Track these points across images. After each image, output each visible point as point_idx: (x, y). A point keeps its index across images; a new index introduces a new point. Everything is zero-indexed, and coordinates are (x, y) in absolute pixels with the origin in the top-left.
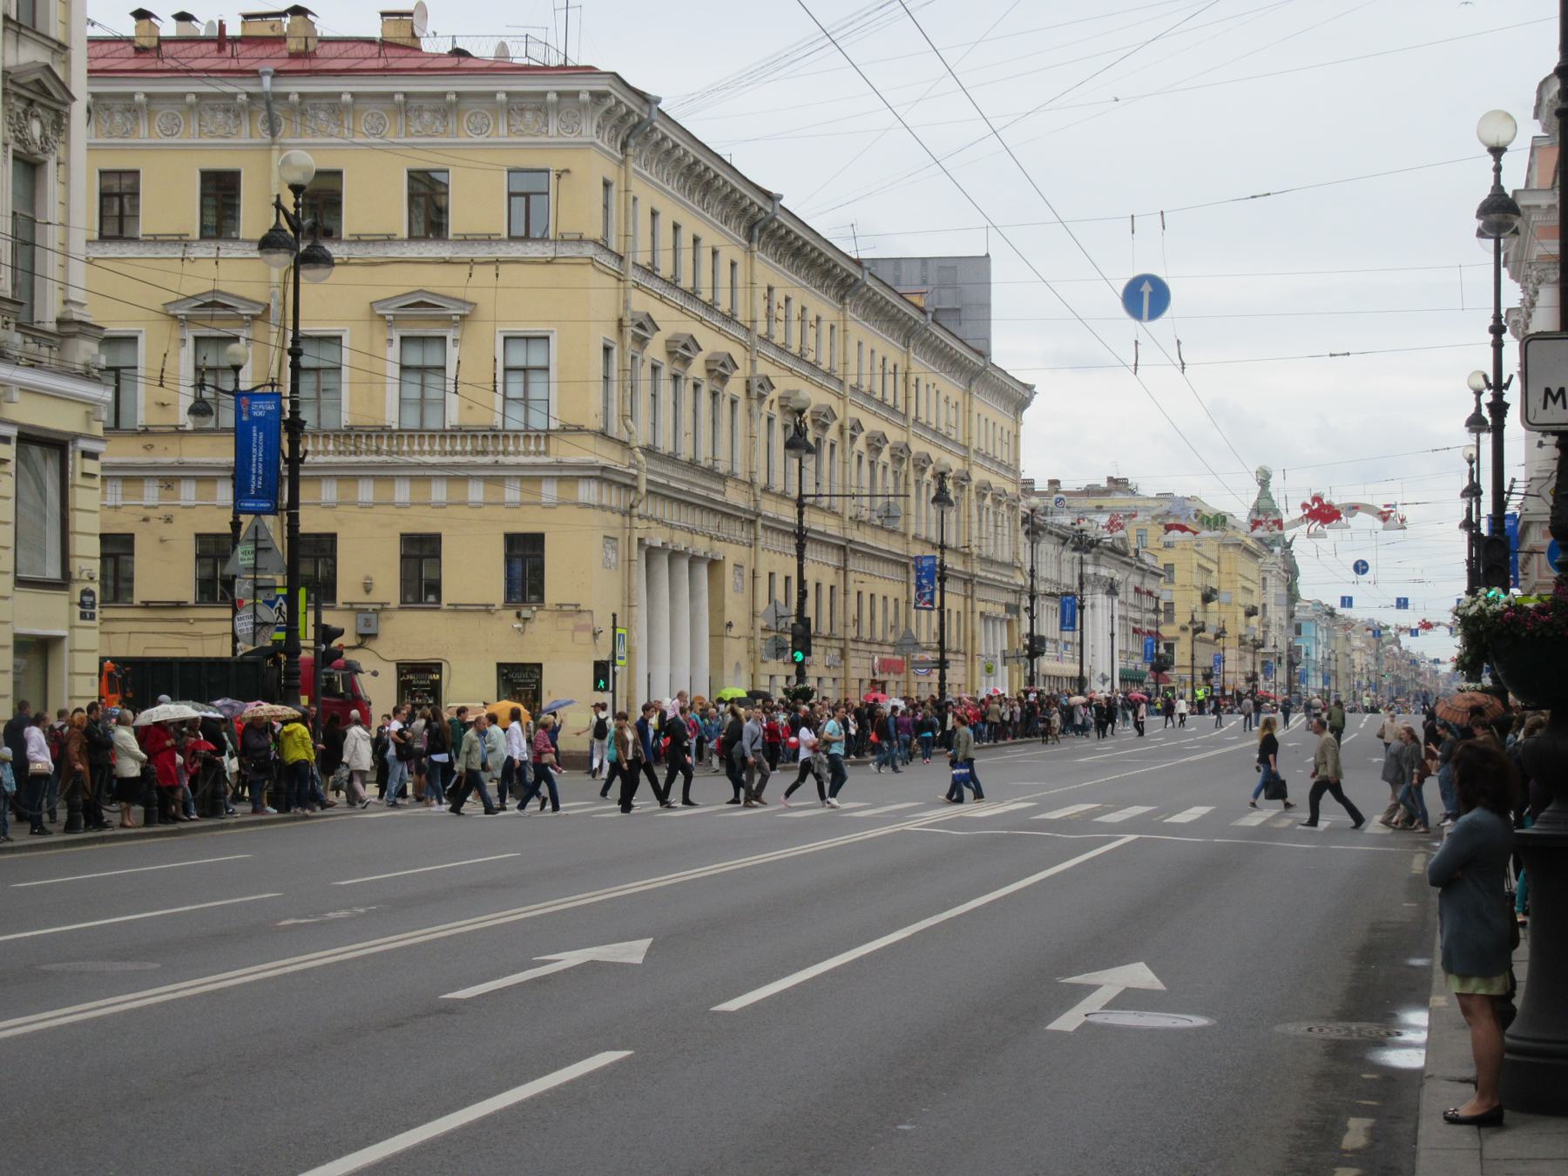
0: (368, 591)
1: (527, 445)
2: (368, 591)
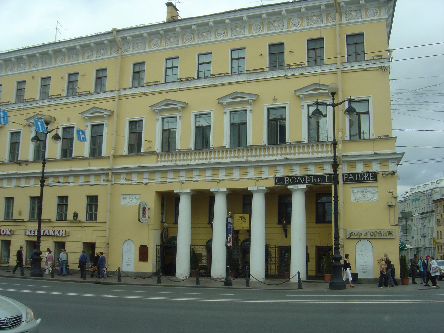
0: (20, 215)
1: (165, 158)
2: (20, 215)
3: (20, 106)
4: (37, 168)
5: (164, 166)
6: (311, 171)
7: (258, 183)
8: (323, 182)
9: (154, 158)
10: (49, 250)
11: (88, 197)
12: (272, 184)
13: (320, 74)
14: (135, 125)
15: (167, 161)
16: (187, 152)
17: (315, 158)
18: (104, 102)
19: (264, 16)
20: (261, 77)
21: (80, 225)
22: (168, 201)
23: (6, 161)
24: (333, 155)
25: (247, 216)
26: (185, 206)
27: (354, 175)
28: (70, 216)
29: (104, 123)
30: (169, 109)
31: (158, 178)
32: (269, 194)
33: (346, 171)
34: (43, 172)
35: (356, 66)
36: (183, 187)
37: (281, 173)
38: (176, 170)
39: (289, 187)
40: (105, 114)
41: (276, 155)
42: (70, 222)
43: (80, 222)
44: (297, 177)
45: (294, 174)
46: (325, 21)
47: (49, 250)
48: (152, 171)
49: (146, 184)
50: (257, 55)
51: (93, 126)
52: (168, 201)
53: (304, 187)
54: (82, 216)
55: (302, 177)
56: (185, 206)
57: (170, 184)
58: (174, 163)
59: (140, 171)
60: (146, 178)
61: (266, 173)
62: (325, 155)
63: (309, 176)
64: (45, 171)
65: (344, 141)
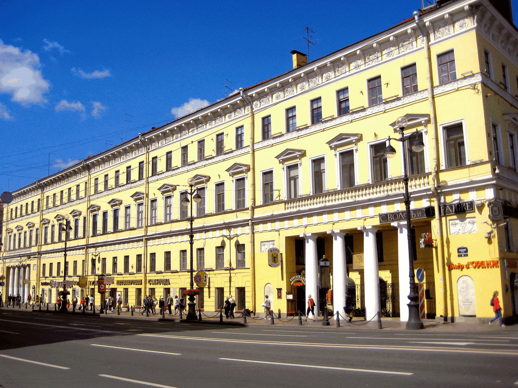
4: (185, 225)
8: (422, 217)
10: (176, 297)
16: (335, 193)
18: (348, 126)
19: (342, 59)
20: (281, 139)
23: (234, 209)
24: (404, 192)
29: (354, 149)
30: (290, 159)
34: (192, 228)
37: (385, 209)
40: (244, 168)
44: (398, 213)
47: (176, 297)
51: (342, 154)
59: (273, 219)
61: (371, 211)
62: (398, 192)
64: (193, 227)
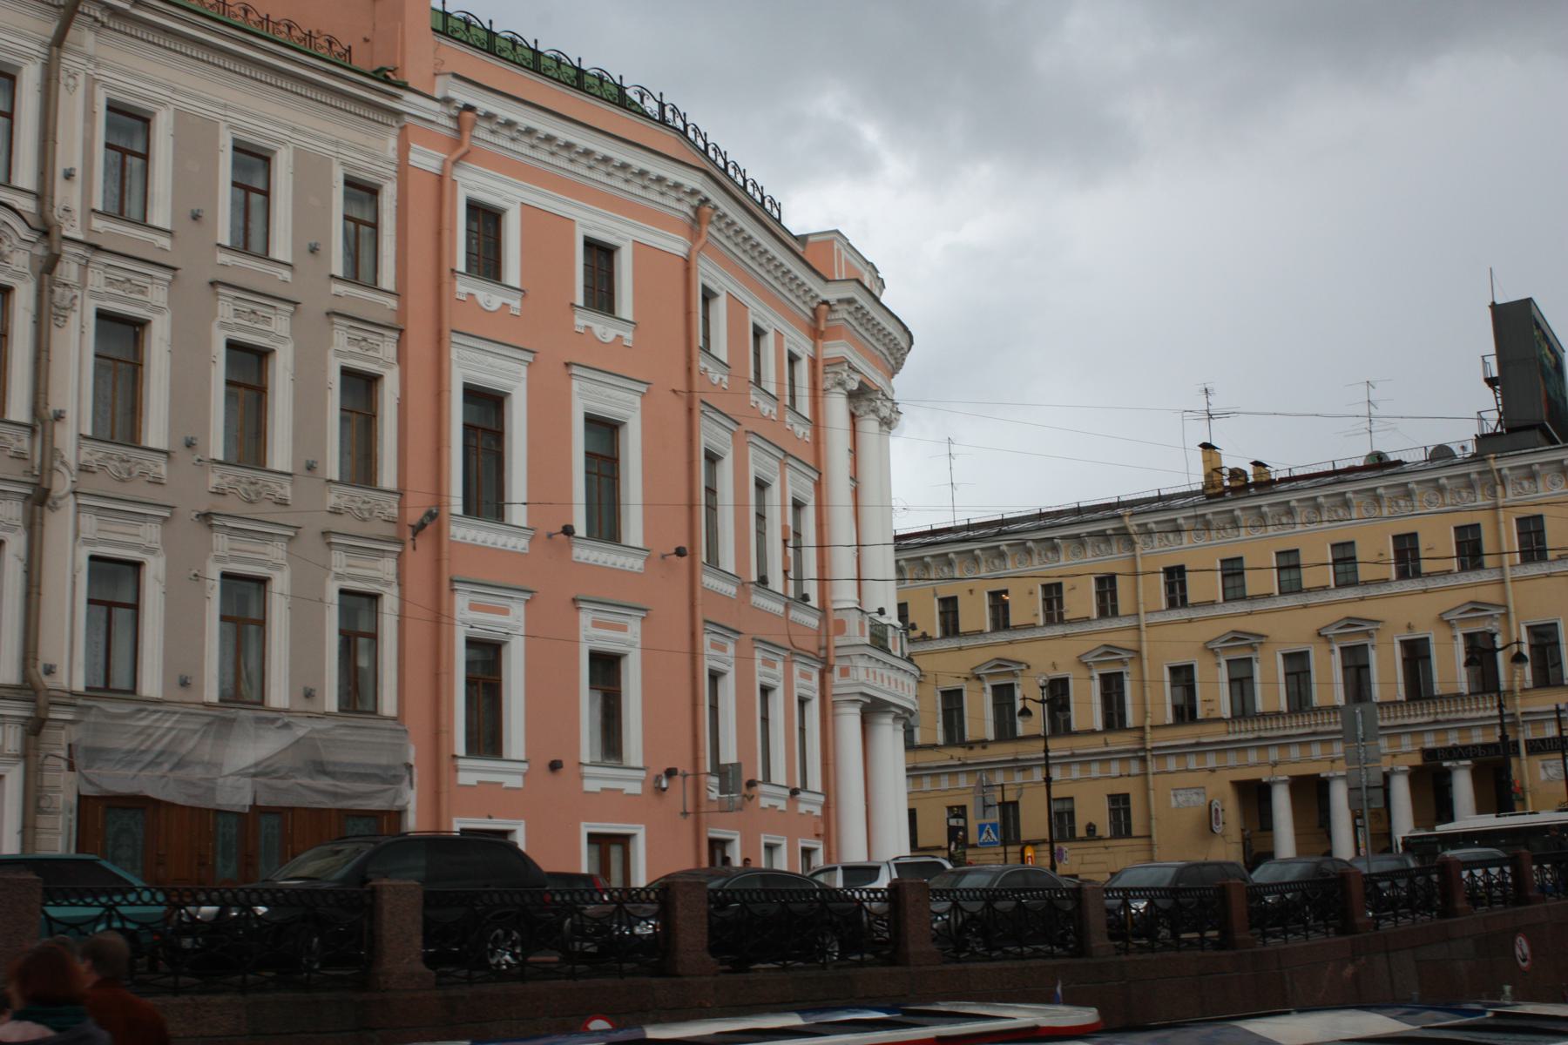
3: (953, 643)
5: (1239, 741)
6: (1477, 738)
7: (1400, 757)
9: (1222, 727)
11: (1109, 796)
12: (1417, 760)
13: (1476, 585)
14: (1183, 676)
15: (1245, 731)
17: (1482, 718)
21: (1101, 843)
22: (1255, 796)
25: (811, 239)
26: (1282, 802)
27: (1543, 741)
28: (1081, 831)
31: (1232, 759)
32: (1415, 776)
33: (1530, 735)
35: (1534, 569)
36: (1279, 768)
37: (1430, 742)
38: (1262, 744)
39: (1446, 764)
41: (1419, 716)
42: (1082, 839)
43: (1100, 838)
45: (1450, 743)
46: (1479, 497)
48: (1221, 748)
49: (1212, 770)
50: (1374, 543)
52: (1255, 796)
53: (1468, 762)
54: (1104, 829)
55: (1465, 748)
56: (1282, 802)
57: (1252, 766)
58: (1255, 735)
59: (1199, 748)
60: (1211, 761)
61: (1407, 743)
63: (1475, 746)
65: (1524, 690)
